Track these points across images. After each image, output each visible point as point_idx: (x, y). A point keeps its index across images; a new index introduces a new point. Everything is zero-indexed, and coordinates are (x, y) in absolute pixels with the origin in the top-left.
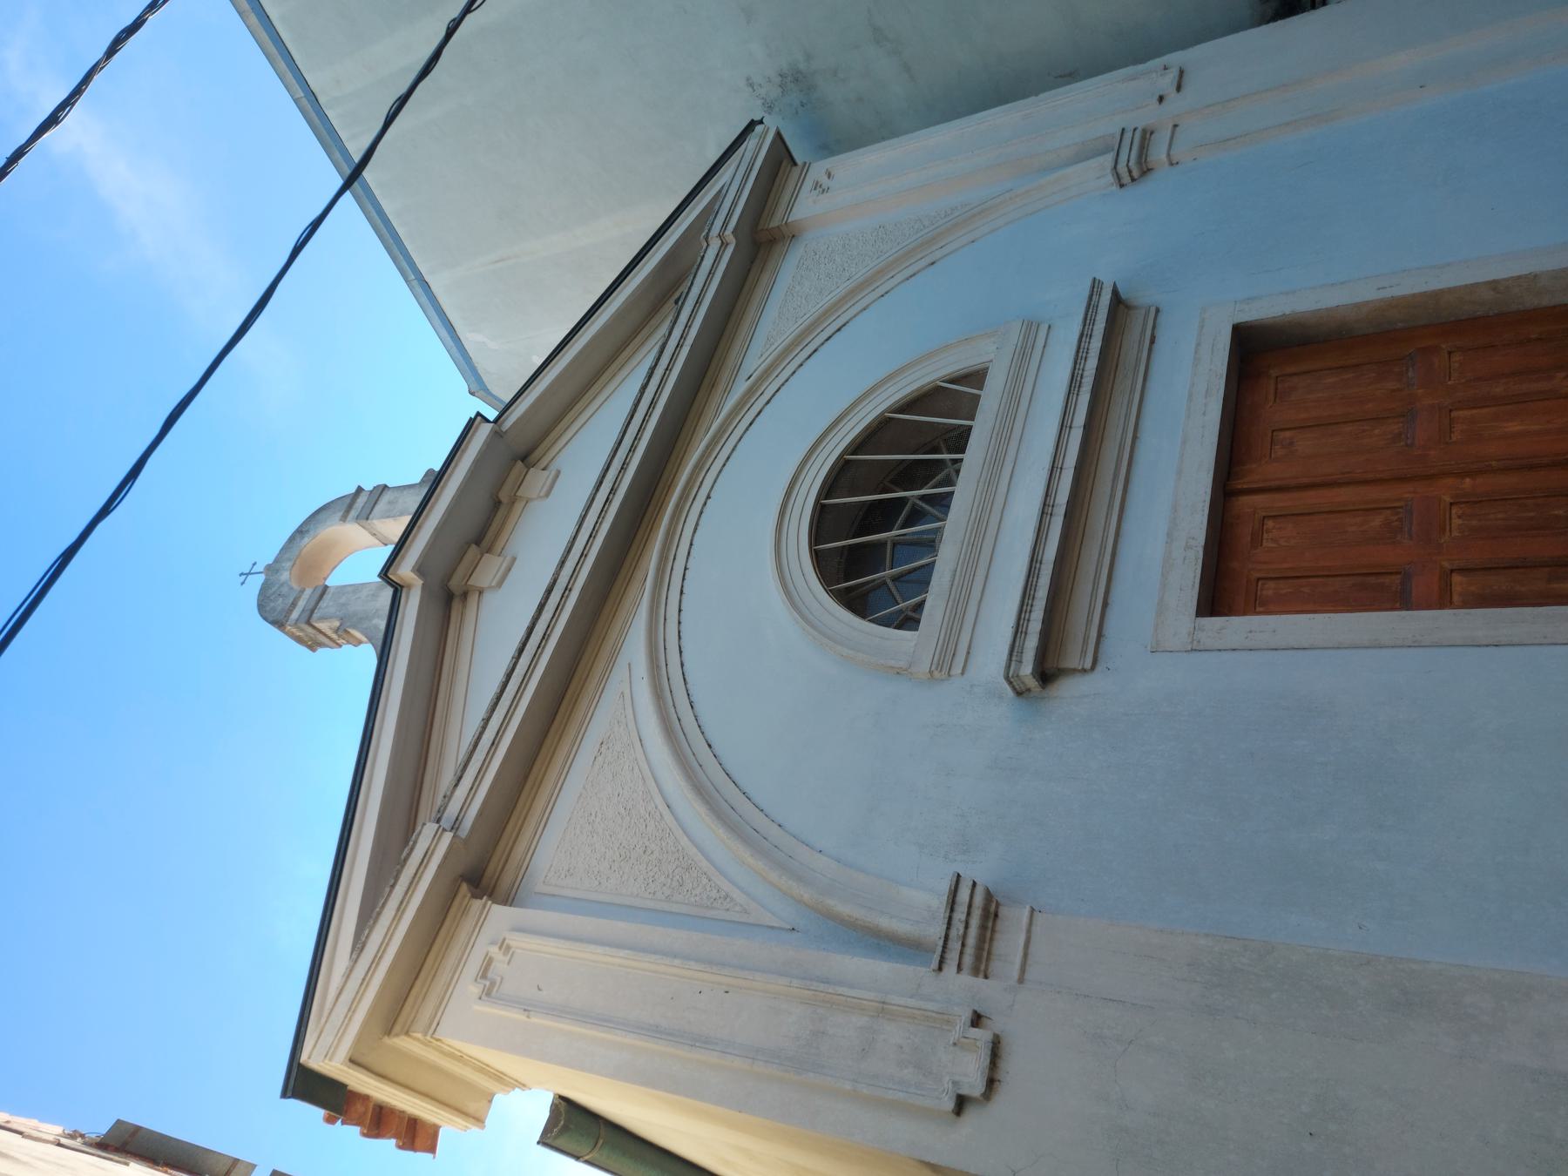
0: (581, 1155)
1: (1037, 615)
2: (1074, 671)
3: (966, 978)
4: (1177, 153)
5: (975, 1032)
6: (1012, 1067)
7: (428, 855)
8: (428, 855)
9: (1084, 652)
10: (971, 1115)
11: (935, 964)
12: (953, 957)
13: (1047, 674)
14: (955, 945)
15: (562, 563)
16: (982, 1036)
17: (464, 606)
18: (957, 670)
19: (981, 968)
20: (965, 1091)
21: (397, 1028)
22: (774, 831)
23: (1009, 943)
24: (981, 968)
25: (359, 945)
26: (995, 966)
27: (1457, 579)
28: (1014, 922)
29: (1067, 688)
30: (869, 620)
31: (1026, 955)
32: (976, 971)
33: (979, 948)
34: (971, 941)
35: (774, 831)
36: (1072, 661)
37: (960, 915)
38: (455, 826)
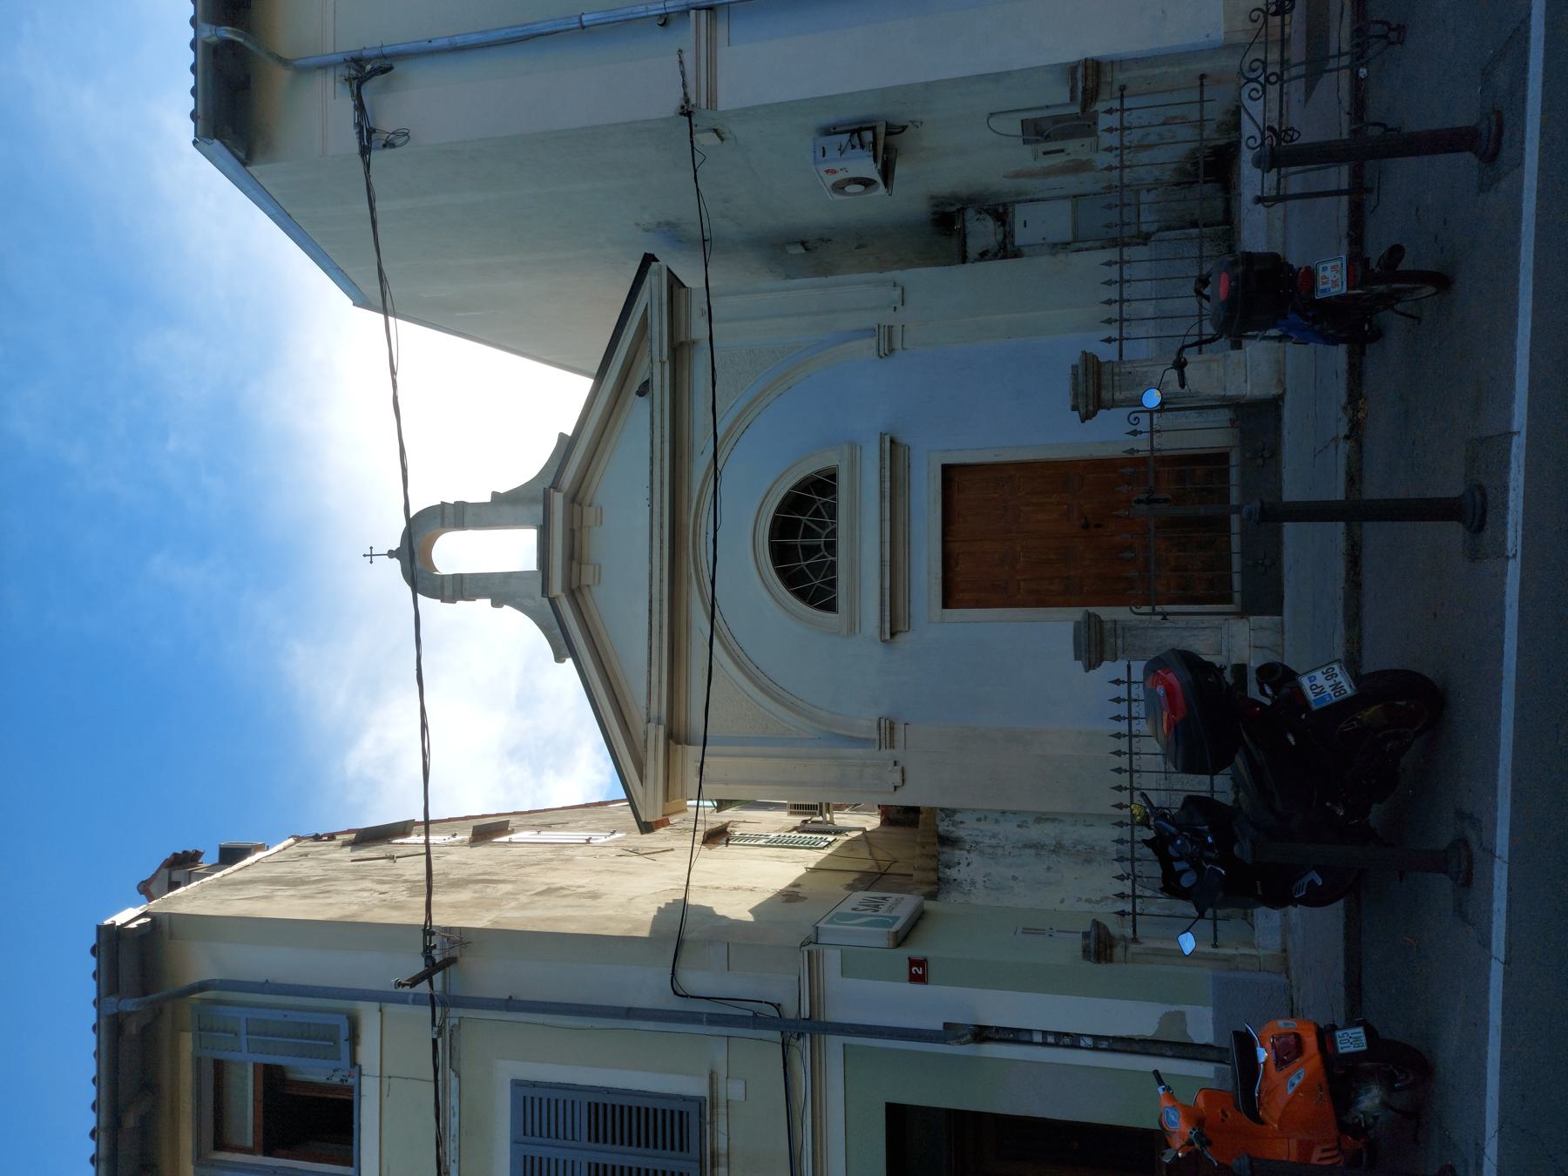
0: (1115, 915)
1: (887, 613)
2: (902, 631)
3: (888, 751)
4: (905, 346)
5: (895, 767)
6: (908, 775)
7: (656, 737)
8: (656, 737)
9: (905, 624)
10: (899, 790)
11: (878, 747)
12: (883, 745)
13: (893, 634)
14: (883, 741)
15: (651, 586)
16: (898, 768)
17: (583, 595)
18: (857, 631)
19: (892, 746)
20: (896, 785)
21: (670, 799)
22: (799, 703)
23: (899, 736)
24: (892, 746)
25: (641, 777)
26: (896, 744)
27: (1022, 583)
28: (900, 727)
29: (900, 638)
30: (816, 607)
31: (905, 740)
32: (890, 747)
33: (890, 740)
34: (888, 739)
35: (799, 703)
36: (901, 628)
37: (883, 731)
38: (659, 719)
